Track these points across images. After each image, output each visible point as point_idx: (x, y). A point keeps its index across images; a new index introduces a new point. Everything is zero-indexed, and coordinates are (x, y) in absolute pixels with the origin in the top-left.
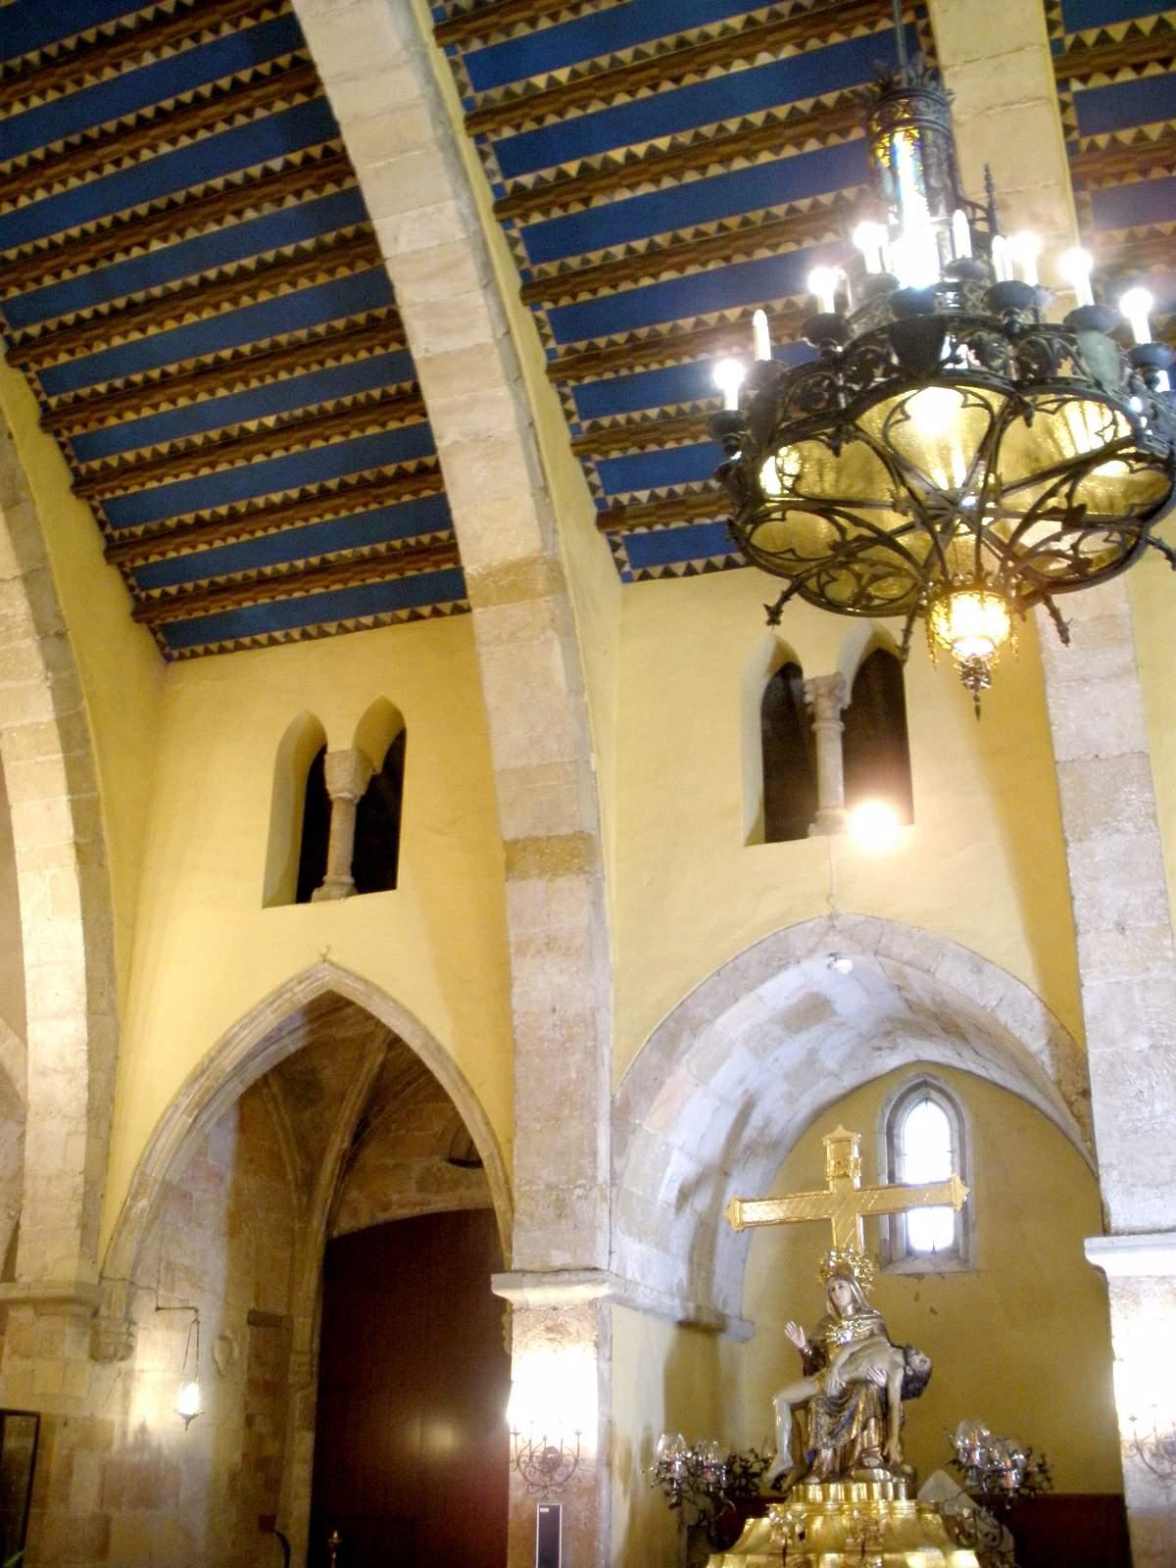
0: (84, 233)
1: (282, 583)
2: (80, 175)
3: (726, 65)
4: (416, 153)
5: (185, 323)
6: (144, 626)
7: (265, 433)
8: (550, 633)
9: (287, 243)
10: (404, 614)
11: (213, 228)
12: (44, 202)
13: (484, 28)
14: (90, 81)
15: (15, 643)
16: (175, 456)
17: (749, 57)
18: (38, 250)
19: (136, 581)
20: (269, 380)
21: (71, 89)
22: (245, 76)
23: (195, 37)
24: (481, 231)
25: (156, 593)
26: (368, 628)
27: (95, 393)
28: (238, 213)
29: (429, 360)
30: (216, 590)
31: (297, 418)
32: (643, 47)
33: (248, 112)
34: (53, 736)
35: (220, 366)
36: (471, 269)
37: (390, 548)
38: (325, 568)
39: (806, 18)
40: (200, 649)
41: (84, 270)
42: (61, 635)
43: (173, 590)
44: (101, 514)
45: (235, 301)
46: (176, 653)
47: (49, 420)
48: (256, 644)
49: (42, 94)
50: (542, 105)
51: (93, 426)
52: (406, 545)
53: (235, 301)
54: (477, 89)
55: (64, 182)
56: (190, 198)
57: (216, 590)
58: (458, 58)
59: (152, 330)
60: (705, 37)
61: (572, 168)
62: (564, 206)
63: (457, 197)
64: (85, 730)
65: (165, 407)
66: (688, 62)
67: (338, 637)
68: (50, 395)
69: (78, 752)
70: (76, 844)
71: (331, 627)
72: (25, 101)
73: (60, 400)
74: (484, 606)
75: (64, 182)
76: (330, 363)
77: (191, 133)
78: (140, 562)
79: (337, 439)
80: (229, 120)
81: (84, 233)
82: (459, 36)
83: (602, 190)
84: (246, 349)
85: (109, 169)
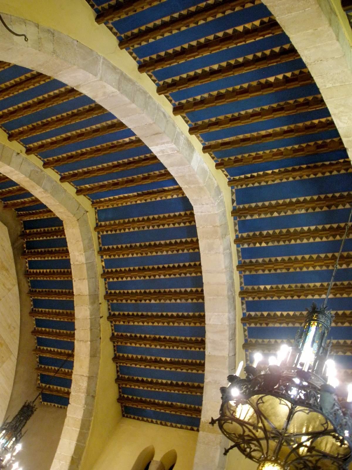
0: (136, 292)
1: (159, 406)
2: (140, 277)
3: (313, 296)
4: (222, 297)
5: (154, 325)
6: (120, 404)
7: (166, 362)
8: (219, 447)
9: (186, 312)
10: (189, 427)
11: (168, 302)
12: (129, 281)
13: (251, 269)
14: (149, 254)
15: (80, 394)
16: (142, 360)
17: (320, 295)
18: (124, 292)
19: (122, 390)
20: (171, 348)
21: (144, 255)
22: (187, 264)
23: (178, 251)
24: (235, 325)
25: (126, 396)
26: (178, 428)
27: (126, 335)
28: (176, 300)
29: (209, 356)
30: (141, 401)
31: (175, 361)
32: (291, 285)
33: (185, 274)
34: (79, 423)
35: (159, 339)
36: (227, 334)
37: (190, 407)
38: (171, 406)
39: (337, 288)
40: (132, 416)
41: (133, 302)
42: (93, 397)
43: (130, 397)
44: (118, 369)
45: (168, 323)
46: (126, 415)
47: (113, 338)
48: (147, 421)
49: (137, 254)
50: (261, 294)
51: (123, 344)
52: (195, 407)
53: (168, 323)
54: (245, 285)
55: (135, 277)
56: (165, 292)
57: (141, 401)
58: (242, 275)
59: (145, 324)
60: (309, 286)
61: (265, 314)
62: (261, 324)
63: (229, 312)
64: (90, 426)
65: (143, 346)
66: (303, 292)
67: (169, 427)
68: (115, 331)
69: (85, 431)
70: (72, 457)
71: (169, 424)
72: (133, 254)
73: (117, 334)
74: (203, 431)
75: (135, 277)
76: (188, 349)
77: (170, 275)
78: (124, 386)
79: (184, 371)
80: (180, 274)
81: (136, 292)
82: (243, 269)
83: (273, 322)
84: (168, 337)
85: (147, 278)
